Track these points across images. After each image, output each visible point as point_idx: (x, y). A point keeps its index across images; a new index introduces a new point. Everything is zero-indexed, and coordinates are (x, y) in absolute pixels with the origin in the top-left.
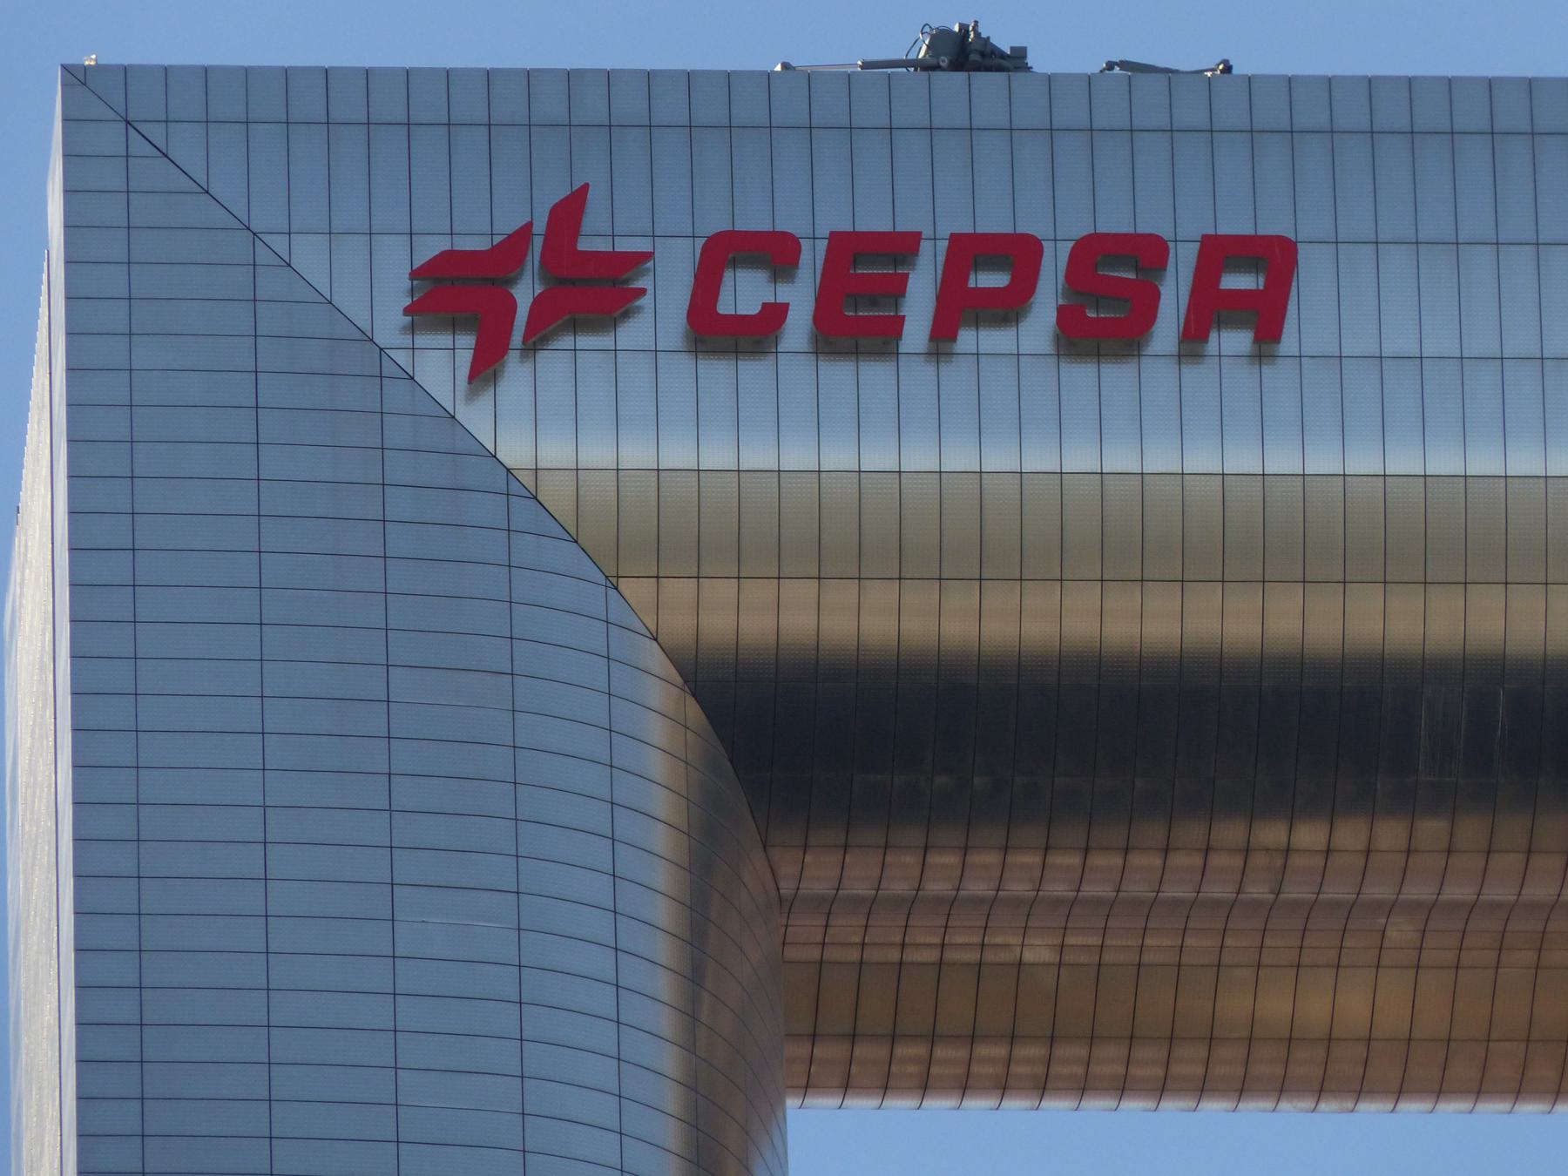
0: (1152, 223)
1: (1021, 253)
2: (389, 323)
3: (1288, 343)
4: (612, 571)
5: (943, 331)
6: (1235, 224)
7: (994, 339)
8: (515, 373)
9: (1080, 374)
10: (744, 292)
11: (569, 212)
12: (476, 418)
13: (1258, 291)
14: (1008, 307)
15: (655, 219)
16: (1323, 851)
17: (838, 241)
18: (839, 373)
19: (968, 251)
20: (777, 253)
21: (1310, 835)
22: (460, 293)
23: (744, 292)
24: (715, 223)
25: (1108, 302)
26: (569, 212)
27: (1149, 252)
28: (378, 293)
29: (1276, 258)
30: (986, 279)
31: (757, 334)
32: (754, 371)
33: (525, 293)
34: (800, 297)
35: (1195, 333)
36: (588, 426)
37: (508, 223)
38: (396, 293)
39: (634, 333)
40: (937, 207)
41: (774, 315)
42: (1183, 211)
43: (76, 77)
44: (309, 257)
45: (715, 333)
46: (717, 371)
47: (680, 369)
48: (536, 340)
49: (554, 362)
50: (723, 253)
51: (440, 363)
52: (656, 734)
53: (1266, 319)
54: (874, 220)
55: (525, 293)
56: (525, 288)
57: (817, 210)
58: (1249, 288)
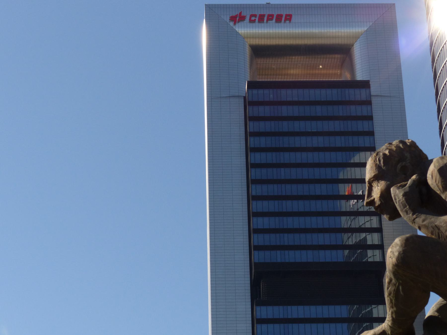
0: (282, 13)
1: (273, 16)
2: (228, 21)
3: (292, 21)
4: (356, 204)
5: (267, 20)
6: (288, 13)
7: (271, 22)
8: (237, 24)
9: (277, 24)
10: (253, 18)
11: (241, 13)
12: (234, 27)
13: (356, 233)
14: (272, 19)
15: (247, 13)
16: (296, 59)
17: (260, 15)
18: (260, 24)
19: (269, 15)
20: (255, 16)
21: (294, 57)
22: (234, 19)
23: (253, 18)
24: (251, 14)
25: (279, 19)
26: (241, 13)
27: (282, 15)
28: (227, 19)
29: (291, 16)
30: (270, 17)
31: (254, 21)
32: (254, 24)
33: (237, 19)
34: (257, 19)
35: (285, 20)
36: (243, 29)
37: (236, 14)
38: (229, 18)
39: (245, 21)
40: (267, 12)
41: (255, 20)
42: (284, 13)
43: (206, 5)
44: (222, 16)
45: (251, 21)
46: (251, 24)
47: (248, 24)
48: (238, 22)
49: (240, 23)
50: (251, 16)
51: (232, 24)
52: (248, 50)
53: (290, 20)
54: (262, 13)
55: (237, 19)
56: (238, 18)
57: (258, 13)
58: (289, 18)
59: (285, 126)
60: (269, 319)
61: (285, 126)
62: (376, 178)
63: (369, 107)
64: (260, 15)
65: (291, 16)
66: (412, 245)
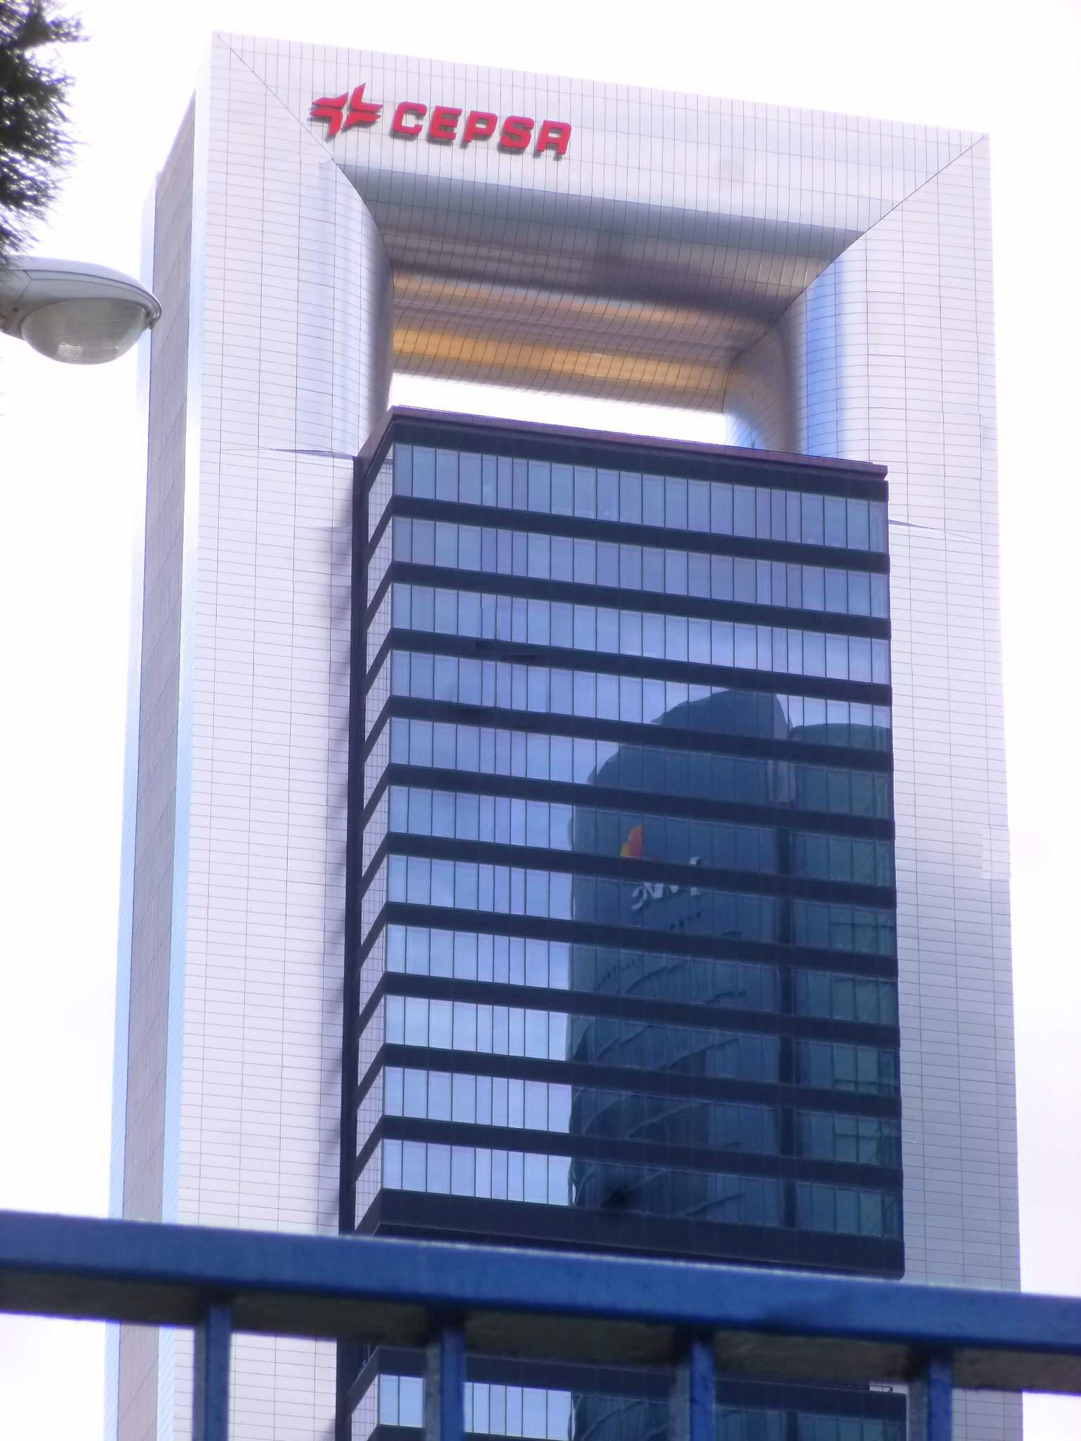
1: (490, 120)
8: (340, 136)
10: (409, 121)
14: (485, 135)
19: (475, 117)
20: (419, 111)
23: (409, 121)
25: (515, 136)
27: (527, 124)
29: (564, 130)
31: (411, 134)
35: (537, 153)
41: (418, 129)
49: (341, 93)
59: (535, 623)
60: (505, 659)
61: (535, 623)
62: (16, 98)
63: (880, 710)
64: (440, 112)
65: (564, 130)
66: (902, 1398)
